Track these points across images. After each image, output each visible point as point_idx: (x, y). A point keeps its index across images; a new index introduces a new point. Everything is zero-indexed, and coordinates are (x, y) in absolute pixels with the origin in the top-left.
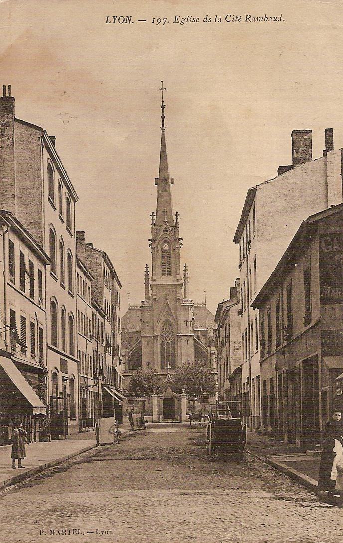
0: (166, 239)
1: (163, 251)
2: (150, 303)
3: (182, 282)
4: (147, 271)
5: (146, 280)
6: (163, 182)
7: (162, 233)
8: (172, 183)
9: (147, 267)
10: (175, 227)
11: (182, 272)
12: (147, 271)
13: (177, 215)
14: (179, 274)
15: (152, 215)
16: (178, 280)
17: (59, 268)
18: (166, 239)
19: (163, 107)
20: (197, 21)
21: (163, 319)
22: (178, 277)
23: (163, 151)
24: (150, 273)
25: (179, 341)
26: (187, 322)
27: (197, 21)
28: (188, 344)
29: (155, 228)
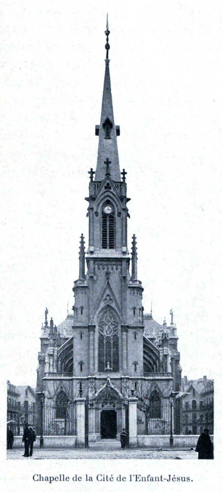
0: (108, 198)
1: (105, 215)
2: (86, 282)
3: (130, 256)
4: (82, 242)
5: (82, 252)
6: (108, 128)
7: (103, 190)
8: (118, 133)
9: (82, 238)
10: (123, 185)
11: (130, 245)
12: (82, 242)
13: (124, 173)
14: (126, 246)
15: (92, 172)
16: (124, 253)
17: (98, 238)
18: (108, 198)
19: (108, 33)
20: (67, 479)
21: (102, 305)
22: (124, 249)
23: (107, 62)
24: (86, 245)
25: (125, 333)
26: (134, 308)
27: (67, 479)
28: (135, 338)
29: (94, 185)
